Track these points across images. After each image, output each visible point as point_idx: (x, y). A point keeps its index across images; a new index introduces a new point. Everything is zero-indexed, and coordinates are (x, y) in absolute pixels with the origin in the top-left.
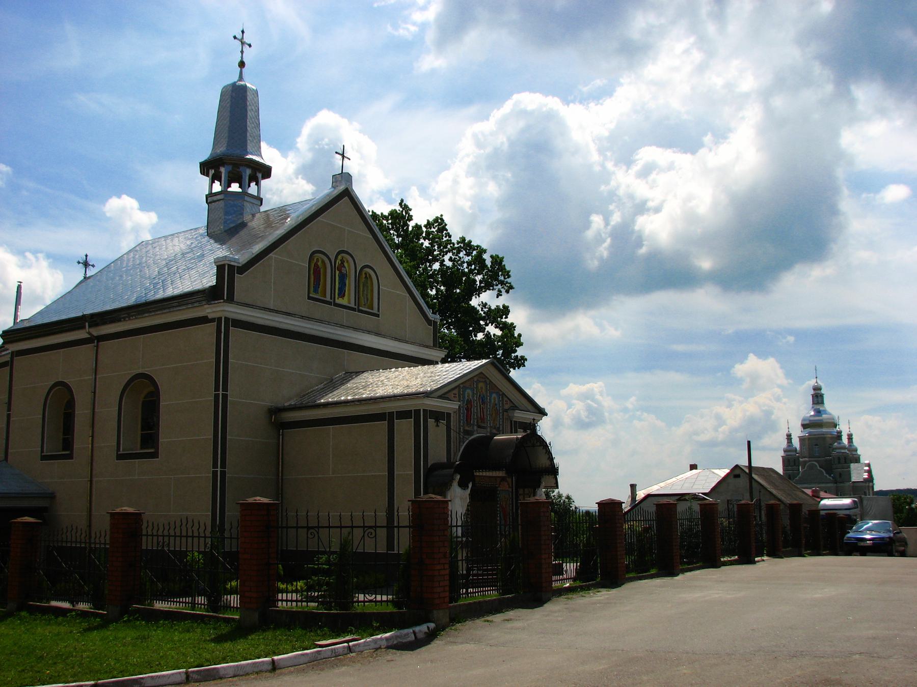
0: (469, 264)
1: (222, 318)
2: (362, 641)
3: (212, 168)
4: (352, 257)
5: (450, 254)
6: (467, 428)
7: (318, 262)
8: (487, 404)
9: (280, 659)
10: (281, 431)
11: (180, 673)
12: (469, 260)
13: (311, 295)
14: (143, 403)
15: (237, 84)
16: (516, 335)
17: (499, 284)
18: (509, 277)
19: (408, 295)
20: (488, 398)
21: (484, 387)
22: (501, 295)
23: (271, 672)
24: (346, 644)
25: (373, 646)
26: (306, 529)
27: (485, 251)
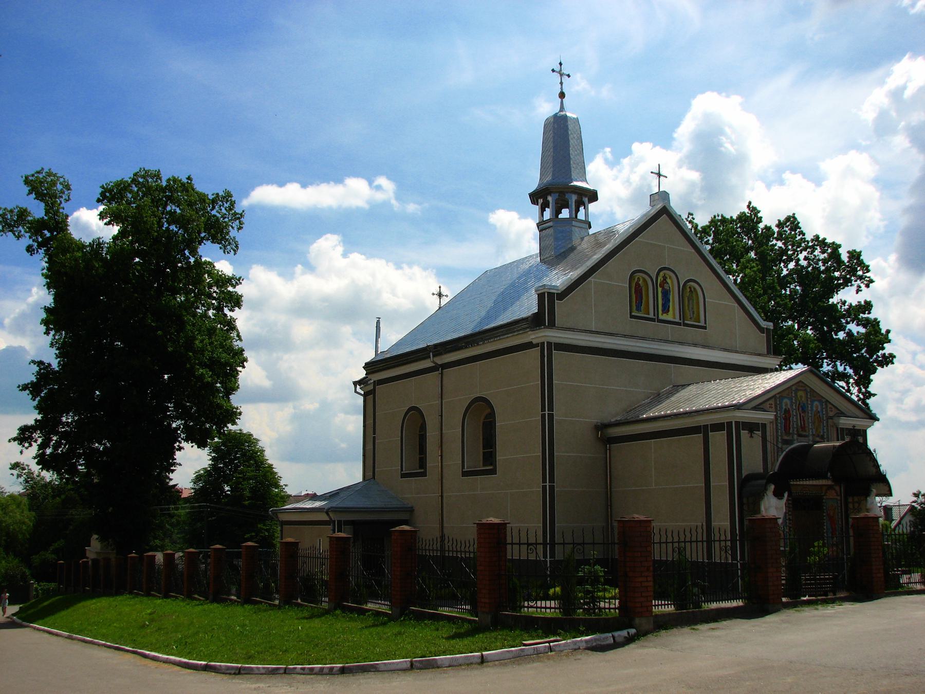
0: (825, 261)
1: (544, 342)
2: (563, 642)
3: (540, 198)
4: (677, 276)
5: (805, 253)
6: (786, 438)
7: (639, 281)
8: (808, 413)
9: (488, 654)
10: (608, 446)
11: (406, 661)
12: (825, 257)
13: (633, 314)
14: (484, 423)
15: (558, 115)
16: (883, 331)
17: (858, 279)
18: (868, 271)
19: (736, 305)
20: (809, 406)
21: (803, 395)
22: (861, 291)
23: (479, 665)
24: (547, 644)
25: (572, 646)
26: (526, 546)
27: (839, 246)
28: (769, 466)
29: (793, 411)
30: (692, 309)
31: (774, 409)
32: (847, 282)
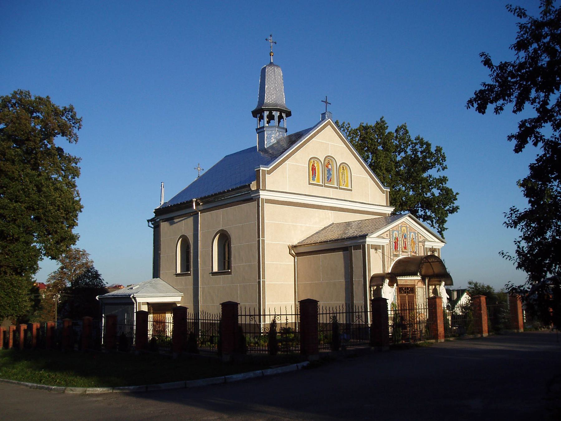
0: (422, 152)
4: (335, 160)
6: (395, 253)
7: (315, 164)
13: (310, 182)
19: (369, 177)
20: (409, 235)
26: (249, 316)
28: (386, 269)
29: (399, 238)
30: (344, 179)
31: (389, 237)
32: (433, 166)
